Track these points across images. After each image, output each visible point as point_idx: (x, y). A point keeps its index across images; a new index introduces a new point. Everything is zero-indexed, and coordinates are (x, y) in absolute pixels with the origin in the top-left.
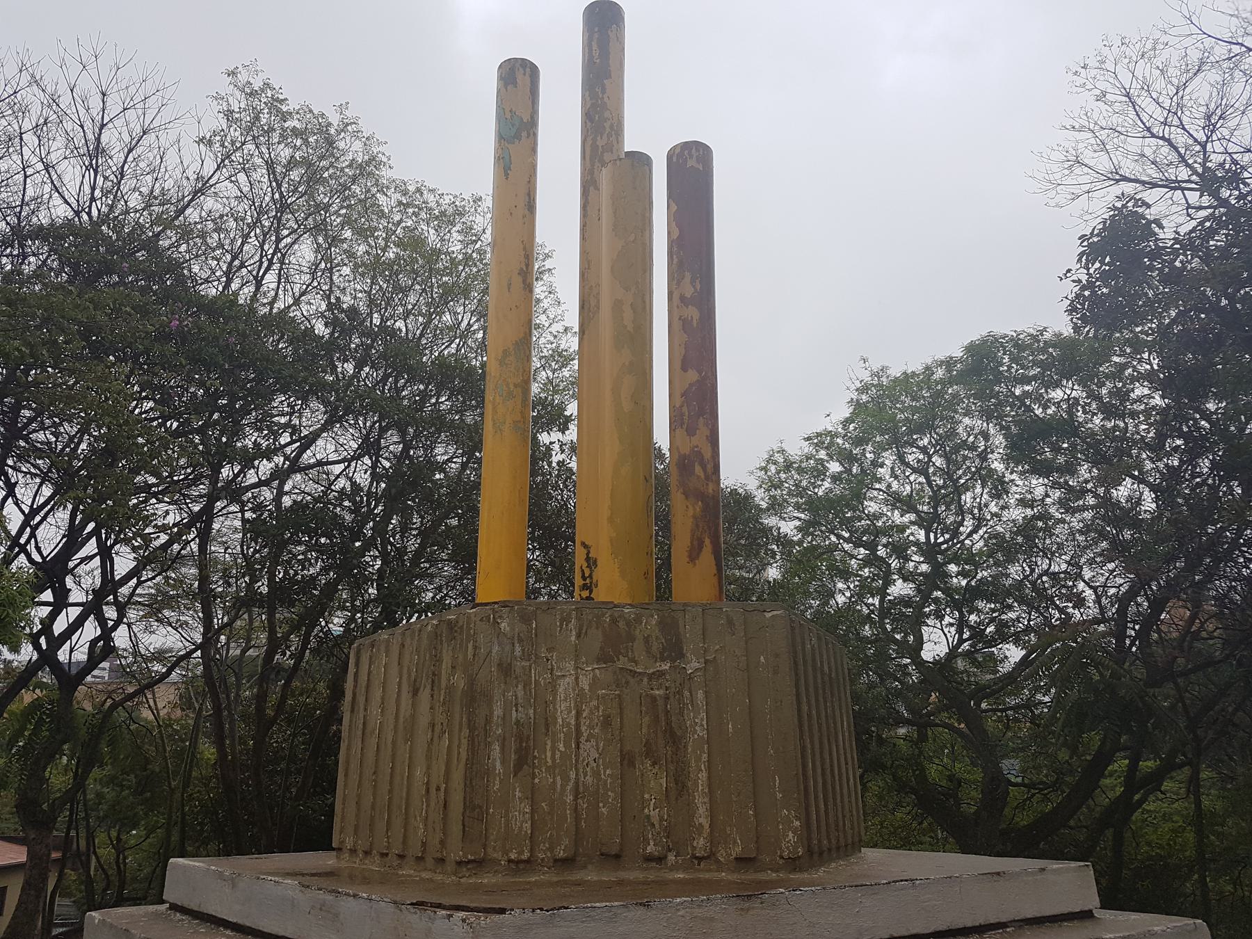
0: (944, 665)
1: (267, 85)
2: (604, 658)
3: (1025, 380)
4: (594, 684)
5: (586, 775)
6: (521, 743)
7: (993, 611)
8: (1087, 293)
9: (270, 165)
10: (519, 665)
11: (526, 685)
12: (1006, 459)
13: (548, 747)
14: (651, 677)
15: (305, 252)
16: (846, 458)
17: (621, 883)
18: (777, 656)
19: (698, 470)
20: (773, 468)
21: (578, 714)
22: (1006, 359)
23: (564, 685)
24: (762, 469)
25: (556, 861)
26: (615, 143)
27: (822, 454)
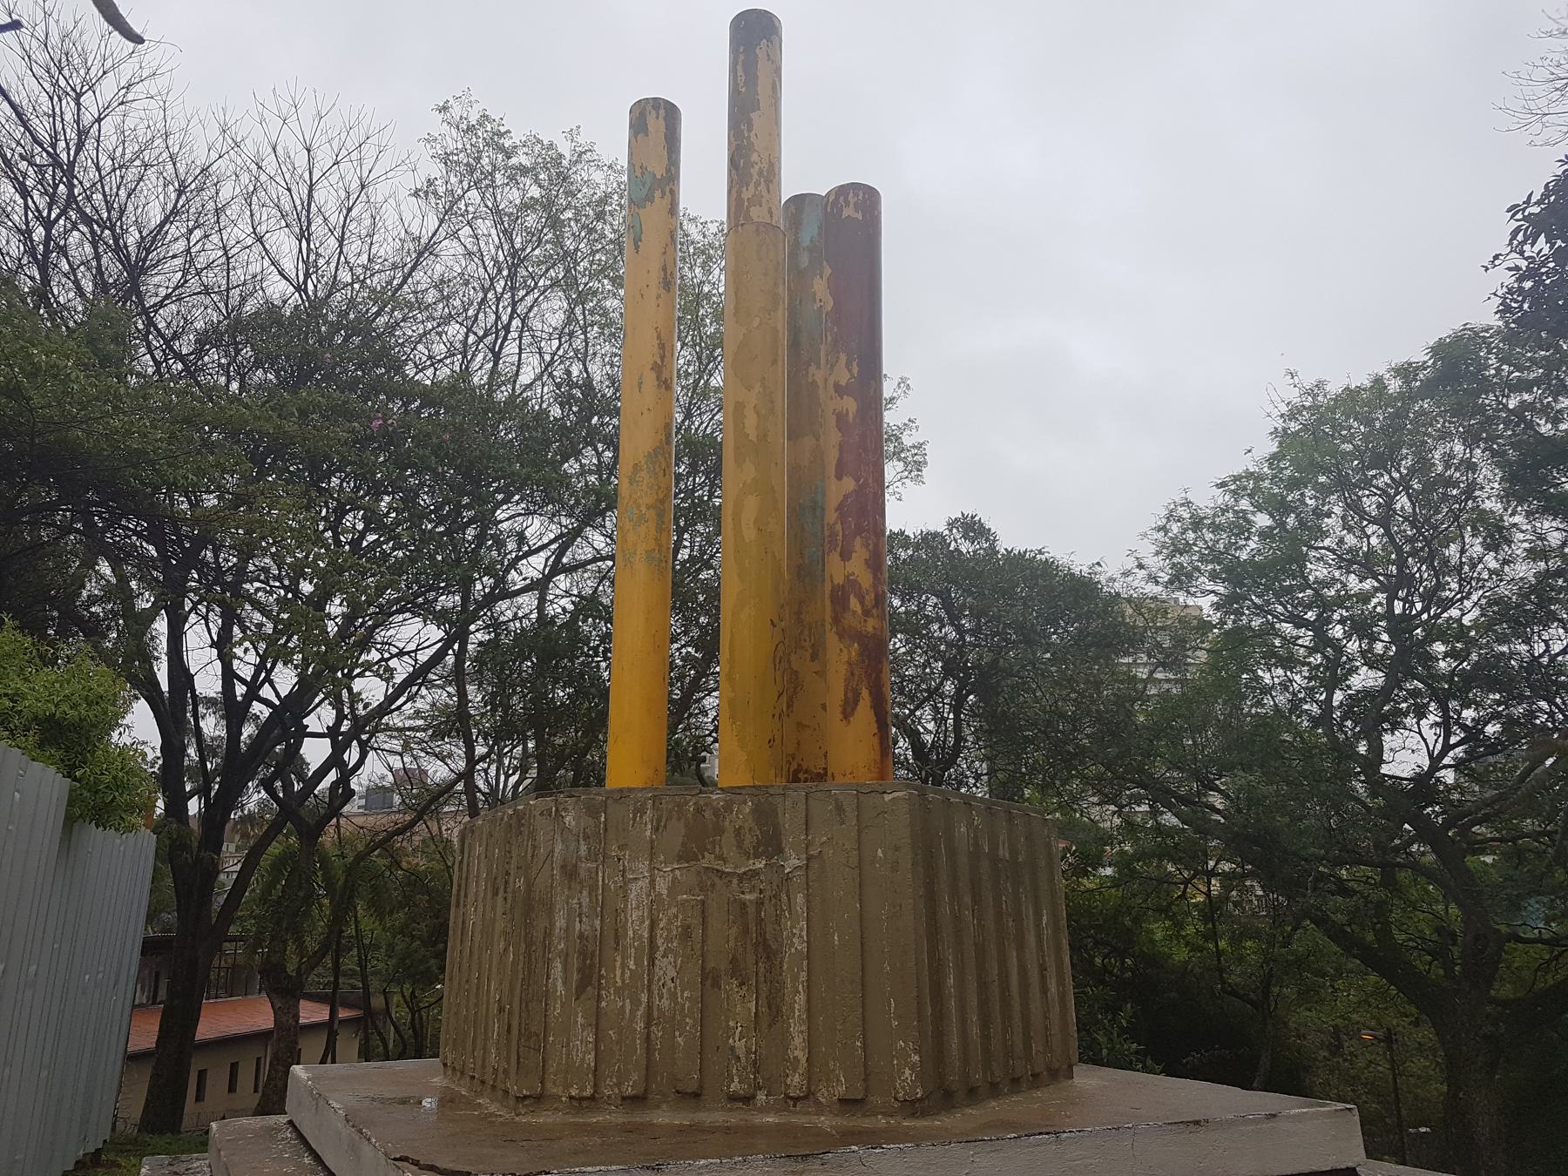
0: (1424, 783)
1: (485, 117)
2: (686, 856)
3: (1526, 386)
4: (674, 887)
5: (661, 997)
6: (584, 961)
7: (1499, 703)
8: (1528, 285)
9: (496, 212)
10: (584, 866)
11: (593, 889)
12: (1506, 497)
13: (618, 964)
14: (741, 877)
15: (553, 311)
16: (1279, 507)
17: (695, 1128)
18: (897, 849)
19: (854, 604)
20: (1175, 528)
21: (653, 925)
22: (1493, 361)
23: (637, 890)
24: (1159, 529)
25: (624, 1098)
26: (765, 193)
27: (1245, 504)
